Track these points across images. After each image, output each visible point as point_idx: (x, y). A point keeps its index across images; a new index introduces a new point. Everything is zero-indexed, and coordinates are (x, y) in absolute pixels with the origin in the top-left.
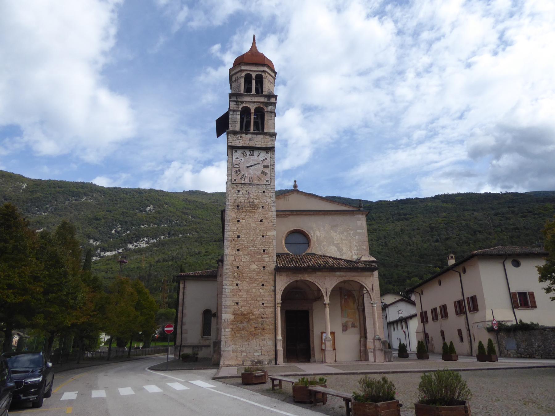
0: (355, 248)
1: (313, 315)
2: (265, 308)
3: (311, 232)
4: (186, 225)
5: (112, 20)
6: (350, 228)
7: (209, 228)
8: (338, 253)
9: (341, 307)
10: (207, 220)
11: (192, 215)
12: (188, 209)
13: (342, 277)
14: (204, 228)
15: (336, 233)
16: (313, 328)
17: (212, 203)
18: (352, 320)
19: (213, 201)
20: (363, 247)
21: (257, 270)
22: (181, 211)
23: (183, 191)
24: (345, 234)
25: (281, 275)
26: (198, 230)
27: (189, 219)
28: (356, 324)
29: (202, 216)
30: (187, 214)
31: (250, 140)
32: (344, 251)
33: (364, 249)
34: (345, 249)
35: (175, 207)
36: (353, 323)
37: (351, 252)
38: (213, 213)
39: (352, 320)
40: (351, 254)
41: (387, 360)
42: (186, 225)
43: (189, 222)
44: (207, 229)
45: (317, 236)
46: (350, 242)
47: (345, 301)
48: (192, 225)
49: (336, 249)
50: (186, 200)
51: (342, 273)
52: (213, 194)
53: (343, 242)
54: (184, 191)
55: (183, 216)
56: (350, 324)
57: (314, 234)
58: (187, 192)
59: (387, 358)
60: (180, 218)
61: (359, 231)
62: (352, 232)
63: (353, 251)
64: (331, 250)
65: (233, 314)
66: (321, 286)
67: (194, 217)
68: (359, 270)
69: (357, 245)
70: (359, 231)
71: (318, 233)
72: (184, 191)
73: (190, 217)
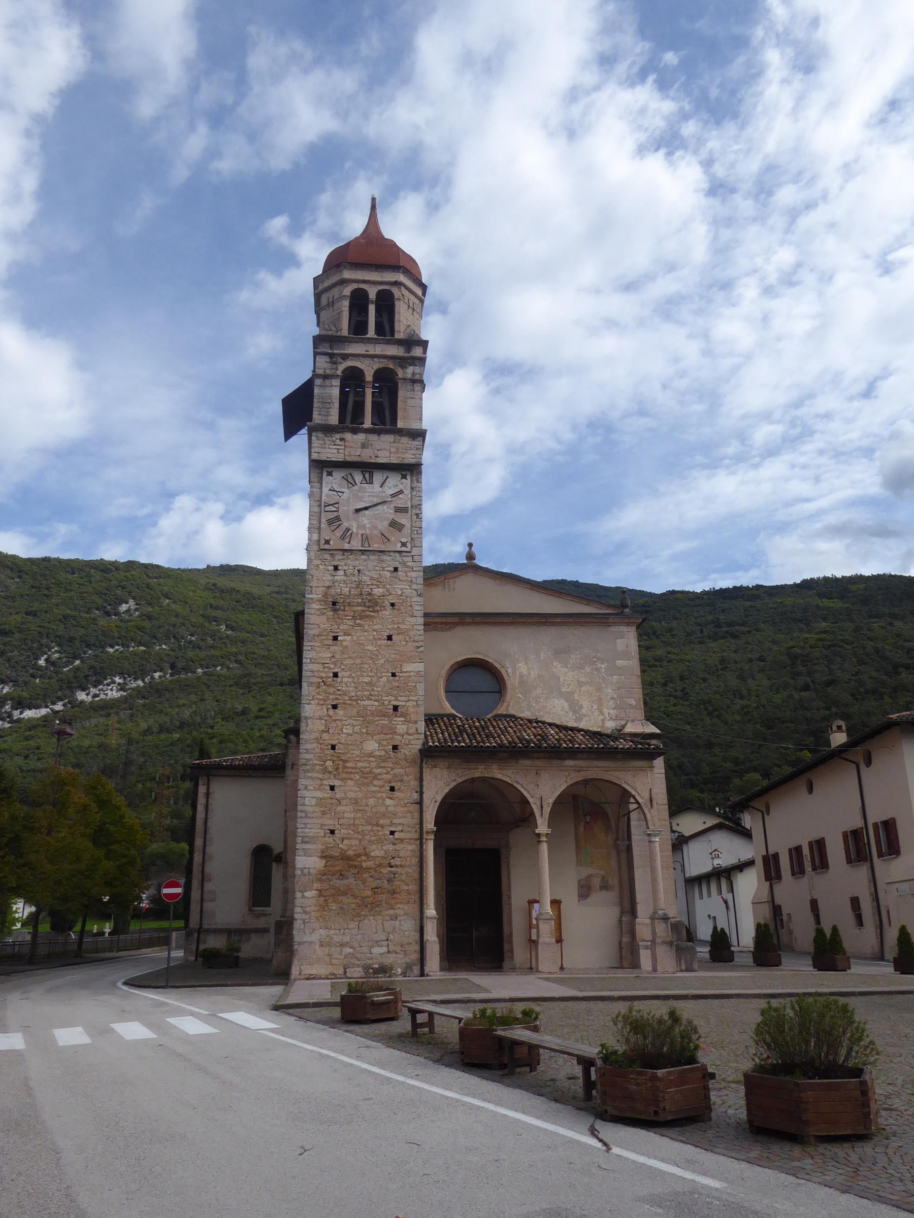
4: (212, 647)
7: (266, 654)
9: (577, 840)
10: (262, 635)
11: (228, 622)
13: (579, 771)
14: (254, 653)
17: (275, 595)
18: (602, 872)
19: (276, 589)
20: (628, 701)
21: (378, 753)
22: (201, 612)
23: (205, 567)
24: (588, 669)
26: (241, 657)
28: (610, 882)
29: (251, 624)
30: (216, 621)
34: (586, 704)
37: (602, 713)
38: (276, 617)
39: (602, 872)
40: (601, 717)
41: (683, 967)
42: (212, 647)
43: (221, 639)
50: (213, 588)
52: (276, 574)
55: (206, 624)
56: (596, 882)
57: (514, 669)
59: (683, 962)
60: (199, 630)
61: (619, 663)
64: (554, 707)
69: (615, 696)
70: (619, 663)
71: (522, 668)
73: (223, 627)
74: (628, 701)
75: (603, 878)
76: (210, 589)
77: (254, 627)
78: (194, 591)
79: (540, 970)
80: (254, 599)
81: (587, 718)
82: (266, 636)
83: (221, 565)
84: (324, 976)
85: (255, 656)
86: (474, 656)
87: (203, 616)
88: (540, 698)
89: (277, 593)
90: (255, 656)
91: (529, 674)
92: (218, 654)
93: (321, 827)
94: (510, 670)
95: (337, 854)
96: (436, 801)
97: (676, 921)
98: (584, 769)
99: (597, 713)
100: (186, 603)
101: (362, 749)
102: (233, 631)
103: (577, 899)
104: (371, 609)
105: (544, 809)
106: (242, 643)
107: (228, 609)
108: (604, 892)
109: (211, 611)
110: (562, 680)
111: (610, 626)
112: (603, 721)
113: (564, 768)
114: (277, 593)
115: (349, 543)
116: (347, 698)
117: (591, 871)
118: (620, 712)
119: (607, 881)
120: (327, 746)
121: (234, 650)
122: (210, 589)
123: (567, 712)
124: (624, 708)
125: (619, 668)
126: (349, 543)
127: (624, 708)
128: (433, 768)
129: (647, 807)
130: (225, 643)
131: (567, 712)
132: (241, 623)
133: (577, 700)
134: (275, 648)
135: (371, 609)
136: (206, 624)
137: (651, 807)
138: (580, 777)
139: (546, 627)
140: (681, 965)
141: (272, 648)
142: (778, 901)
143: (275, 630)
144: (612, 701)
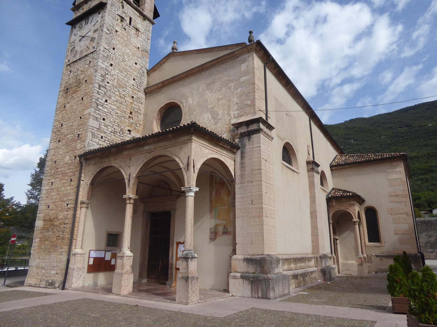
0: (236, 107)
1: (176, 218)
2: (68, 210)
3: (184, 101)
4: (349, 148)
5: (276, 13)
6: (231, 78)
7: (370, 147)
8: (212, 120)
9: (211, 202)
10: (368, 141)
11: (354, 139)
12: (349, 135)
13: (150, 152)
14: (365, 148)
15: (212, 92)
16: (174, 237)
17: (371, 126)
18: (224, 222)
19: (372, 123)
20: (246, 102)
21: (69, 162)
22: (343, 137)
23: (344, 121)
24: (224, 90)
25: (89, 165)
26: (360, 150)
27: (351, 143)
28: (229, 229)
29: (363, 138)
30: (349, 139)
31: (83, 9)
32: (219, 117)
33: (247, 105)
34: (220, 112)
35: (338, 135)
36: (225, 227)
37: (229, 115)
38: (372, 133)
39: (224, 222)
40: (229, 118)
41: (260, 295)
42: (349, 148)
43: (352, 145)
44: (369, 148)
45: (189, 105)
46: (229, 100)
47: (216, 194)
48: (355, 147)
49: (210, 116)
50: (346, 128)
51: (151, 147)
52: (371, 118)
53: (220, 103)
54: (345, 121)
55: (346, 141)
56: (221, 229)
57: (187, 102)
58: (347, 121)
59: (260, 291)
60: (344, 143)
61: (242, 79)
62: (233, 84)
63: (232, 113)
64: (204, 119)
65: (44, 220)
66: (125, 173)
67: (356, 141)
68: (170, 135)
69: (238, 102)
70: (242, 79)
71: (190, 101)
72: (345, 121)
73: (352, 141)
74: (246, 102)
75: (225, 226)
76: (345, 129)
77: (364, 139)
78: (340, 131)
79: (112, 292)
80: (363, 129)
81: (221, 121)
82: (369, 141)
83: (350, 120)
84: (33, 285)
85: (366, 149)
86: (169, 102)
87: (344, 138)
88: (197, 116)
89: (372, 125)
90: (366, 149)
91: (193, 103)
92: (352, 150)
93: (46, 204)
94: (184, 104)
95: (48, 219)
96: (87, 185)
97: (261, 258)
98: (153, 150)
99: (227, 115)
100: (337, 135)
101: (64, 161)
102: (356, 141)
103: (208, 240)
104: (78, 87)
105: (130, 182)
106: (360, 145)
107: (353, 134)
108: (225, 236)
109: (347, 136)
110: (209, 101)
111: (238, 57)
112: (230, 120)
113: (144, 152)
114: (372, 125)
115: (76, 57)
116: (63, 136)
117: (219, 222)
118: (240, 112)
119: (227, 228)
120: (53, 162)
121: (358, 148)
122: (345, 129)
123: (210, 120)
124: (243, 108)
125: (242, 82)
126: (76, 57)
127: (243, 108)
128: (89, 165)
129: (185, 170)
130: (354, 146)
131: (210, 120)
132: (359, 138)
133: (216, 111)
134: (373, 144)
135: (78, 87)
136: (346, 141)
137: (188, 170)
138: (149, 156)
139: (203, 72)
140: (258, 293)
141: (372, 145)
142: (77, 255)
143: (373, 138)
144: (236, 106)
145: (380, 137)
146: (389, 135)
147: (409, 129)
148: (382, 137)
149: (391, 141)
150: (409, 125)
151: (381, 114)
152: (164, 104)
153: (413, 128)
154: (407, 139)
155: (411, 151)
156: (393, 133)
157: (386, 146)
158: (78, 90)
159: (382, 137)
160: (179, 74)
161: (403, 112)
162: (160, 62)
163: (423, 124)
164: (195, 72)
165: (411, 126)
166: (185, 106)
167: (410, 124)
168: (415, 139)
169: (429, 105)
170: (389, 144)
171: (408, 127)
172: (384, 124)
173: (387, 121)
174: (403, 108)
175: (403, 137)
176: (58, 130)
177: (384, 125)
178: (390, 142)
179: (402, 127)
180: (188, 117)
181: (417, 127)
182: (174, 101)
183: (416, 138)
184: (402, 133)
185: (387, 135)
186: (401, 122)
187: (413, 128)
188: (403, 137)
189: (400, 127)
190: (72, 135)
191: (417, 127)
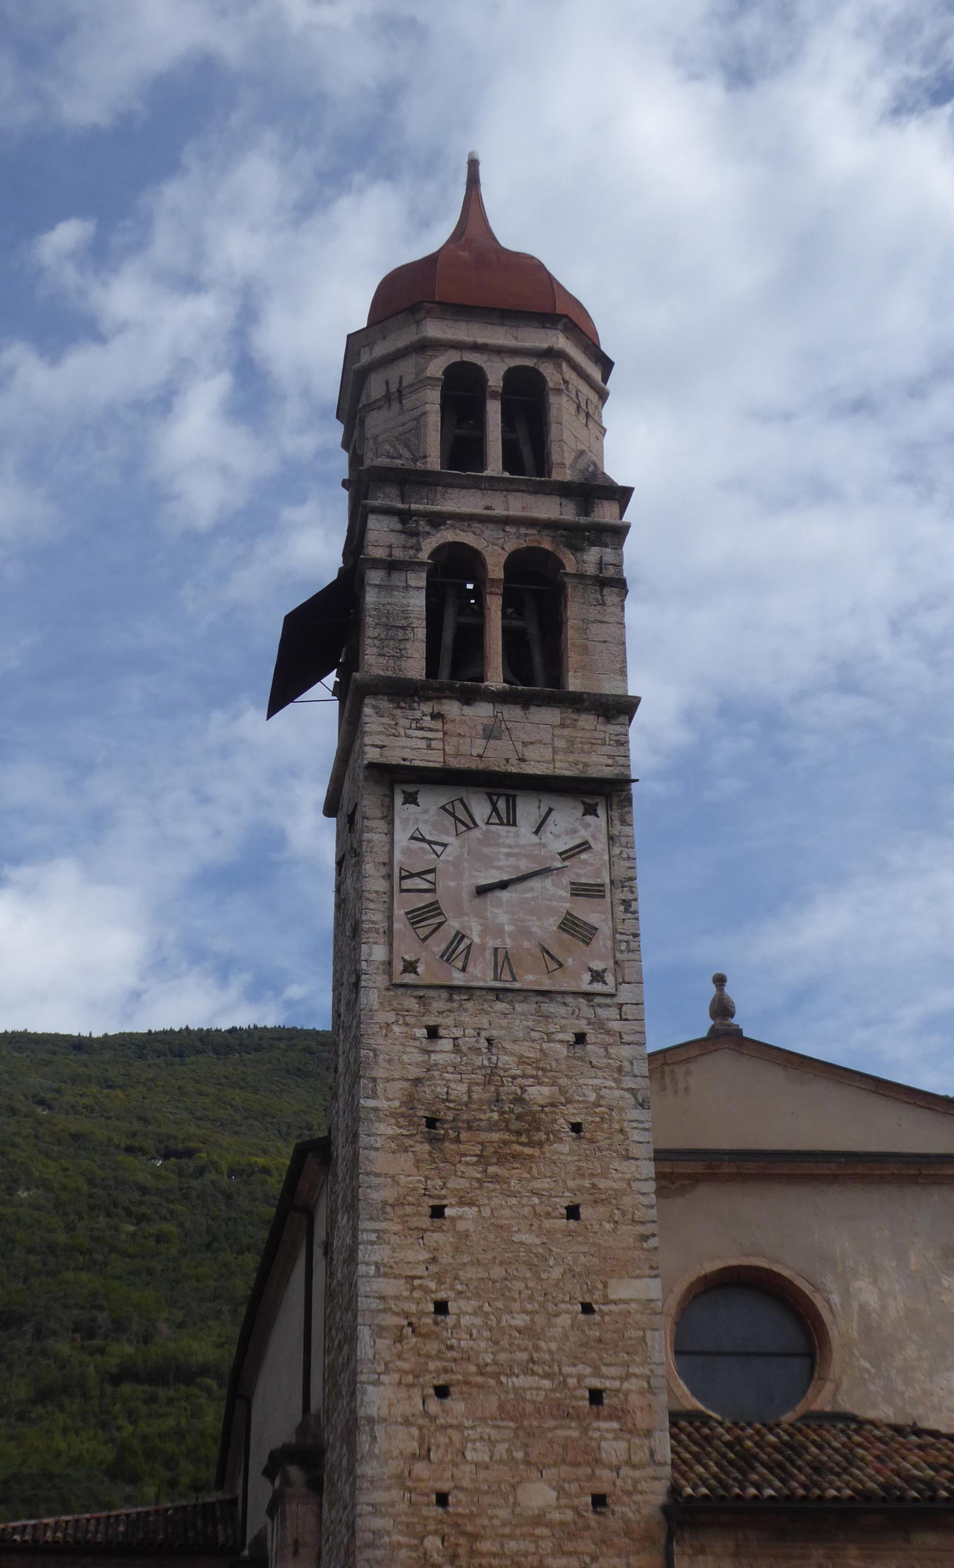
3: (829, 1282)
57: (847, 1294)
86: (745, 1261)
91: (884, 1308)
115: (464, 970)
145: (10, 1191)
146: (64, 1188)
147: (181, 1173)
148: (23, 1194)
149: (70, 1228)
150: (180, 1147)
151: (31, 1030)
152: (719, 1265)
153: (200, 1172)
154: (160, 1238)
155: (181, 1325)
156: (91, 1182)
157: (32, 1258)
158: (531, 1157)
159: (23, 1194)
160: (777, 1147)
161: (159, 1054)
162: (667, 1054)
163: (261, 1161)
164: (881, 1176)
165: (189, 1153)
166: (838, 1308)
167: (192, 1145)
168: (208, 1246)
169: (308, 1050)
170: (52, 1249)
171: (173, 1160)
172: (42, 1102)
173: (58, 1091)
174: (165, 1032)
175: (141, 1219)
176: (410, 1324)
177: (42, 1112)
178: (62, 1238)
179: (144, 1152)
180: (866, 1364)
181: (224, 1167)
182: (775, 1269)
183: (216, 1245)
184: (144, 1190)
185: (56, 1185)
186: (140, 1118)
187: (200, 1172)
188: (141, 1219)
189: (130, 1150)
190: (547, 1383)
191: (224, 1167)
